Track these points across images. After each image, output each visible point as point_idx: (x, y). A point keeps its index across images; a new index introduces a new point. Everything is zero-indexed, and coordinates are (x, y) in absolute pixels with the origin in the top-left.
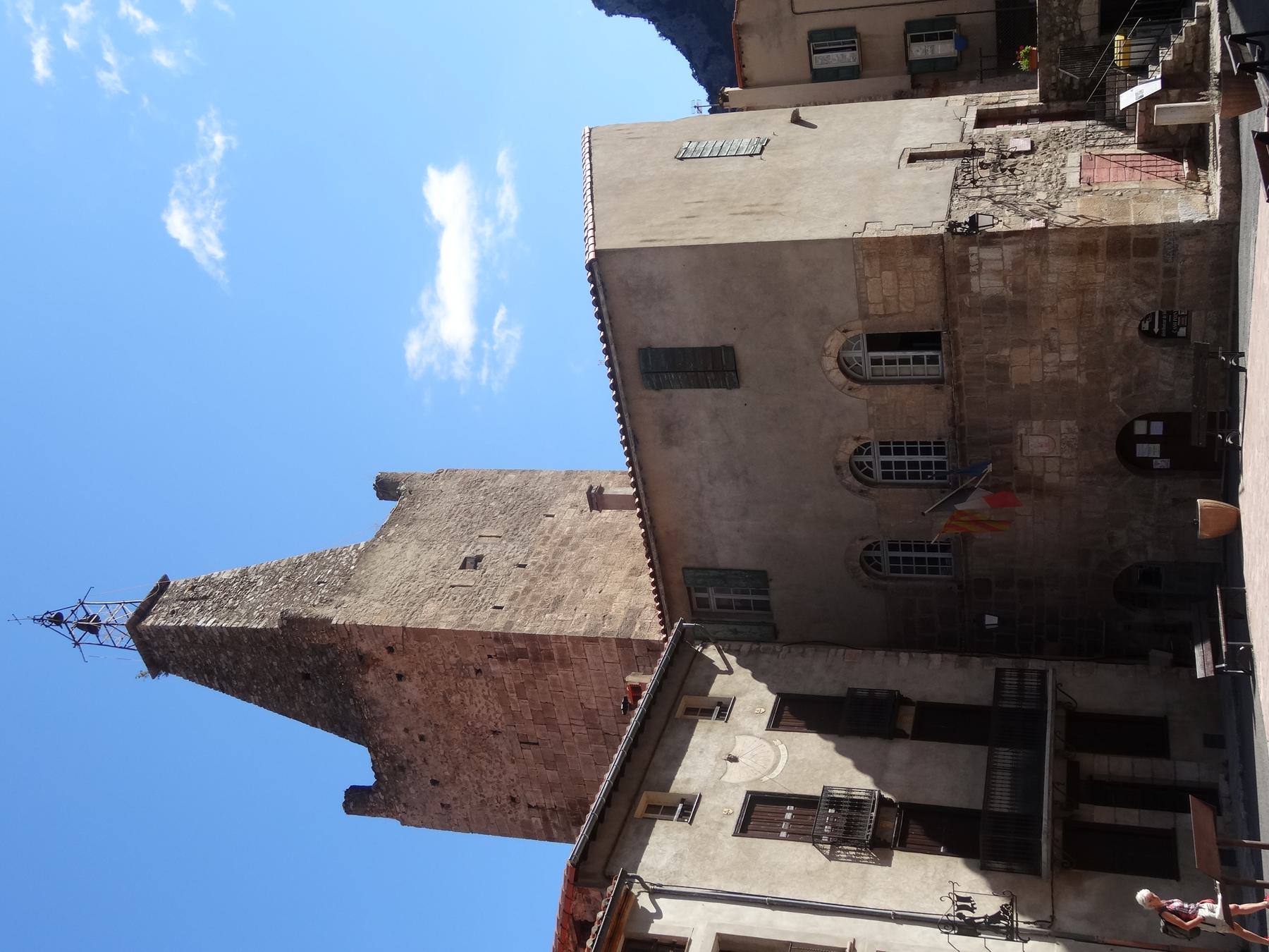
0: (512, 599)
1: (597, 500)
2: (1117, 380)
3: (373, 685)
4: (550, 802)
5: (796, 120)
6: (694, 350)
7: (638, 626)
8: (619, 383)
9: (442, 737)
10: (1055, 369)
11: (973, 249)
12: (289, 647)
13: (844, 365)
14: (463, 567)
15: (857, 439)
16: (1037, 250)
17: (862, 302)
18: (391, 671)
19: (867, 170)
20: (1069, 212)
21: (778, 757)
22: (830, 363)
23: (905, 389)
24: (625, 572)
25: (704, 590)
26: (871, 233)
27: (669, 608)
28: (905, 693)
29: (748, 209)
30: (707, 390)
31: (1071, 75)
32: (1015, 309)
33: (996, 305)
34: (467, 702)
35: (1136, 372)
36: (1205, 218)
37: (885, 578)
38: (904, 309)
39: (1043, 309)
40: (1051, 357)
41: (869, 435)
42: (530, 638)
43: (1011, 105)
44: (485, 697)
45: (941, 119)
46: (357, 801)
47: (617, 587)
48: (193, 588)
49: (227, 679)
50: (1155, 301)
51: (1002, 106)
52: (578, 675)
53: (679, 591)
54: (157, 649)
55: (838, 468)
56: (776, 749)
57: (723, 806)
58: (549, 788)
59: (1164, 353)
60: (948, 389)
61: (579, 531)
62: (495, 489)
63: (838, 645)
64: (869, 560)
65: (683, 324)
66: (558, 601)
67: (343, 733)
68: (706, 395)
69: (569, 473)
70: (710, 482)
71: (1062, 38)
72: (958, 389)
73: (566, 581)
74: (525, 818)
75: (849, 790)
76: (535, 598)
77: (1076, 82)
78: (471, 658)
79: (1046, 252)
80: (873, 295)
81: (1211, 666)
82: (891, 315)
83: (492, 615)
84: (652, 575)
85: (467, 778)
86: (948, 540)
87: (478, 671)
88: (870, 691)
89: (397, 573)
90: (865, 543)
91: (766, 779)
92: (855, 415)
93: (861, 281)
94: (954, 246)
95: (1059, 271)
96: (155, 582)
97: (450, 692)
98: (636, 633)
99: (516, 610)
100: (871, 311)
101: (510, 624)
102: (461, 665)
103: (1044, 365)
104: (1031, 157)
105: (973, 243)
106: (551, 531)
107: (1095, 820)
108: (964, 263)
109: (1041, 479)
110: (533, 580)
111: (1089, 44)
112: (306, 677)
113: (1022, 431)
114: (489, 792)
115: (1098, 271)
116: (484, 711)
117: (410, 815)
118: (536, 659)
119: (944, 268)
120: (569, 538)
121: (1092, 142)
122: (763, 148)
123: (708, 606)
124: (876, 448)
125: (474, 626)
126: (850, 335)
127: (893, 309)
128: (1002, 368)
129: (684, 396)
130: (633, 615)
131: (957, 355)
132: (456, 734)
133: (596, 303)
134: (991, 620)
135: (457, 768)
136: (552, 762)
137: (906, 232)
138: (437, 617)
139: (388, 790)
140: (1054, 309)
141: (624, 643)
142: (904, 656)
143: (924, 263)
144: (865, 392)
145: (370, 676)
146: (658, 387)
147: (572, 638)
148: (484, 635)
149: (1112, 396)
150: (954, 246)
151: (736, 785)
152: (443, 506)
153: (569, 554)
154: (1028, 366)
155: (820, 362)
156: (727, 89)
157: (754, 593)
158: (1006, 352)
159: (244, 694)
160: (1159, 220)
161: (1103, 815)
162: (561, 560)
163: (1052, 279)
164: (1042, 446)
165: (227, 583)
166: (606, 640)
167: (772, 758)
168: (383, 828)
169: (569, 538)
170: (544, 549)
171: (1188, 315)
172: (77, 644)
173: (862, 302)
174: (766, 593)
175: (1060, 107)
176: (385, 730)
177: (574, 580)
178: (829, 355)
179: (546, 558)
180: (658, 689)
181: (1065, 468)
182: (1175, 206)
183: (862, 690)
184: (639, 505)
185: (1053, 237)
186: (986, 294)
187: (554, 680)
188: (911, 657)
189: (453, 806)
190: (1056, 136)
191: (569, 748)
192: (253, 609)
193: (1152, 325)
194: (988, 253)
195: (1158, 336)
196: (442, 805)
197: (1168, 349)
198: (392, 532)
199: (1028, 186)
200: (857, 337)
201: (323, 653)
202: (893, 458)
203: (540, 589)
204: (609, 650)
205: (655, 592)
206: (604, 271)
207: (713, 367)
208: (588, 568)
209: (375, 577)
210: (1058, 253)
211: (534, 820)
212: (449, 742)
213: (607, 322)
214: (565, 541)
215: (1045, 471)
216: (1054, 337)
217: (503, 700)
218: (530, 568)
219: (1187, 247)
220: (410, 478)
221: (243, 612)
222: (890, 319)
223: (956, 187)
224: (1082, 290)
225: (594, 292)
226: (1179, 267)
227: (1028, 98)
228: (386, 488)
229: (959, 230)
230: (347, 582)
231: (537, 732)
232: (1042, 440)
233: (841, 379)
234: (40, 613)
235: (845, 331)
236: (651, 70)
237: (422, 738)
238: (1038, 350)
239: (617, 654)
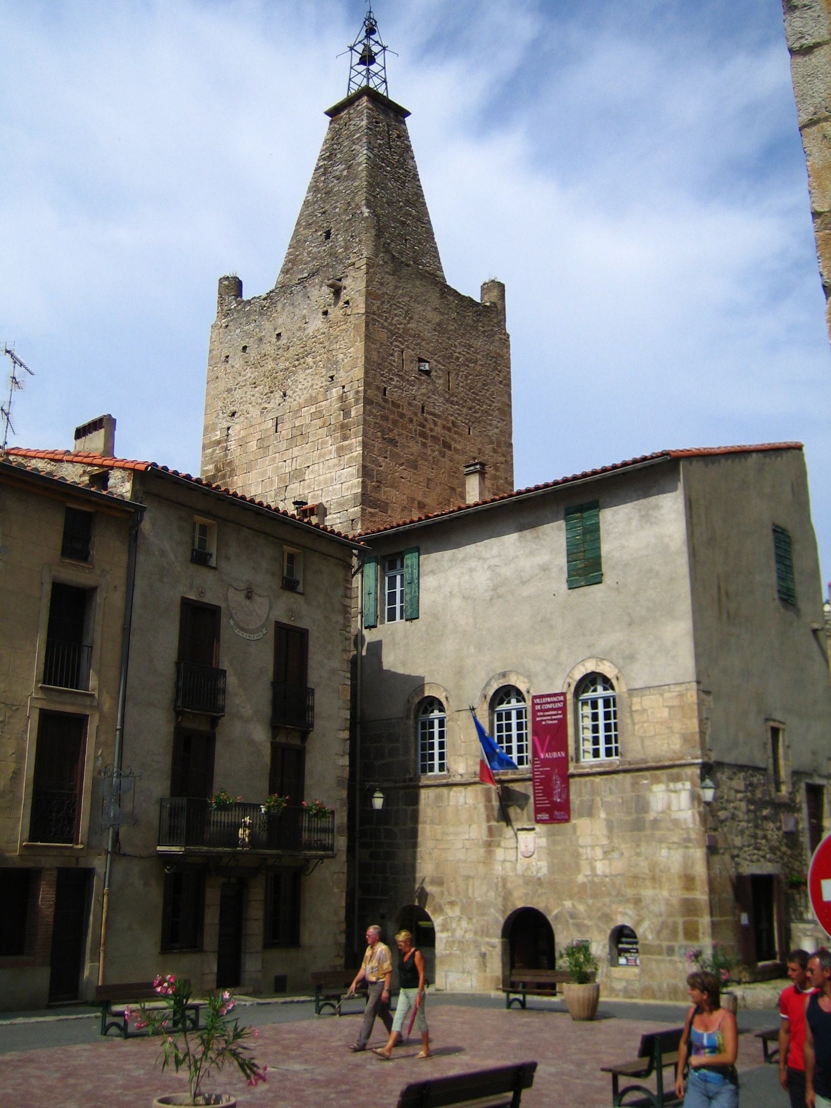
2: (581, 908)
4: (232, 445)
6: (599, 548)
7: (372, 510)
10: (590, 856)
11: (688, 785)
16: (688, 840)
28: (312, 735)
29: (723, 591)
30: (565, 560)
33: (642, 806)
34: (308, 371)
35: (587, 922)
37: (416, 718)
38: (637, 727)
39: (638, 846)
40: (599, 852)
41: (620, 688)
50: (646, 938)
54: (349, 113)
55: (504, 675)
57: (208, 588)
63: (353, 678)
66: (393, 442)
68: (562, 560)
70: (489, 567)
76: (395, 422)
79: (687, 847)
80: (649, 701)
82: (632, 716)
83: (378, 388)
85: (249, 375)
87: (332, 377)
88: (312, 708)
100: (635, 700)
103: (593, 847)
105: (693, 784)
106: (456, 433)
109: (499, 846)
110: (411, 420)
112: (328, 235)
116: (300, 386)
118: (343, 427)
120: (450, 448)
126: (614, 682)
127: (637, 718)
134: (378, 802)
139: (238, 311)
140: (638, 854)
142: (346, 734)
149: (568, 904)
151: (226, 599)
157: (402, 607)
158: (603, 815)
161: (213, 897)
162: (429, 442)
163: (664, 852)
169: (450, 448)
170: (438, 430)
172: (352, 48)
174: (402, 618)
178: (597, 665)
187: (326, 443)
188: (345, 740)
189: (228, 366)
191: (274, 459)
196: (227, 357)
202: (514, 721)
203: (404, 427)
210: (686, 858)
216: (616, 855)
217: (312, 401)
222: (628, 715)
231: (285, 430)
234: (375, 15)
235: (617, 679)
237: (279, 335)
238: (605, 842)
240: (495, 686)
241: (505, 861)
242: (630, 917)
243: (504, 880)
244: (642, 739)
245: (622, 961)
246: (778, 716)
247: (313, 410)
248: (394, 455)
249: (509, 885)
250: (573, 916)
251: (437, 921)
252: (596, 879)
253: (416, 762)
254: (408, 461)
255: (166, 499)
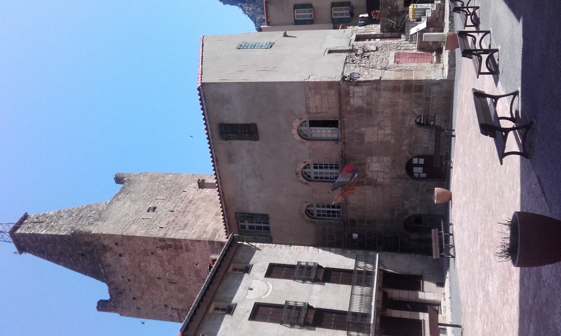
0: (167, 224)
1: (202, 185)
2: (406, 141)
3: (109, 258)
5: (285, 35)
6: (240, 124)
8: (210, 137)
9: (137, 280)
11: (351, 87)
12: (76, 242)
13: (300, 133)
14: (148, 211)
15: (305, 162)
16: (376, 89)
17: (308, 107)
18: (117, 253)
19: (312, 56)
20: (389, 76)
21: (269, 289)
22: (294, 132)
23: (324, 143)
24: (213, 215)
25: (244, 222)
26: (312, 79)
27: (229, 228)
29: (264, 69)
31: (392, 22)
32: (367, 112)
33: (360, 110)
34: (148, 266)
36: (442, 78)
37: (315, 218)
40: (381, 132)
41: (309, 161)
42: (174, 240)
43: (369, 33)
44: (155, 264)
45: (343, 37)
46: (103, 306)
47: (210, 220)
48: (37, 218)
49: (50, 255)
51: (366, 33)
52: (193, 255)
53: (233, 221)
55: (297, 174)
56: (268, 285)
58: (181, 301)
59: (425, 131)
60: (341, 143)
61: (196, 197)
62: (163, 181)
64: (309, 211)
65: (237, 115)
66: (186, 225)
67: (97, 278)
68: (245, 143)
69: (193, 175)
70: (246, 178)
71: (389, 7)
72: (344, 143)
73: (190, 217)
74: (171, 313)
75: (296, 302)
76: (177, 224)
77: (395, 25)
78: (149, 248)
79: (380, 89)
80: (312, 105)
81: (438, 254)
83: (159, 231)
84: (223, 215)
86: (339, 204)
87: (152, 253)
89: (121, 213)
90: (307, 204)
91: (263, 297)
92: (305, 154)
93: (307, 99)
94: (344, 86)
95: (385, 97)
96: (21, 215)
97: (141, 262)
98: (217, 239)
99: (169, 229)
100: (311, 111)
101: (166, 234)
102: (145, 250)
103: (378, 134)
104: (376, 52)
105: (351, 85)
106: (185, 197)
107: (393, 316)
108: (348, 93)
109: (376, 180)
110: (176, 217)
111: (400, 10)
112: (83, 255)
113: (369, 161)
114: (156, 303)
115: (400, 98)
116: (155, 270)
117: (124, 311)
118: (176, 248)
119: (340, 95)
120: (191, 201)
121: (399, 48)
122: (271, 46)
123: (245, 228)
124: (312, 166)
125: (151, 235)
126: (303, 120)
127: (319, 111)
128: (362, 135)
129: (236, 144)
130: (216, 231)
131: (344, 129)
132: (143, 278)
133: (201, 104)
135: (143, 293)
136: (182, 290)
137: (325, 79)
138: (136, 231)
140: (383, 112)
141: (211, 243)
143: (332, 92)
144: (308, 143)
145: (108, 255)
146: (226, 139)
147: (190, 240)
148: (155, 238)
149: (404, 148)
150: (344, 86)
152: (143, 186)
153: (191, 206)
154: (372, 135)
155: (290, 131)
156: (262, 26)
157: (263, 223)
158: (363, 129)
159: (57, 262)
160: (424, 78)
161: (396, 313)
163: (382, 100)
164: (377, 167)
165: (52, 217)
166: (204, 241)
167: (266, 288)
168: (113, 317)
170: (182, 205)
171: (435, 116)
173: (308, 107)
174: (268, 223)
175: (389, 34)
176: (114, 277)
177: (193, 217)
179: (182, 208)
180: (222, 260)
181: (385, 176)
182: (430, 73)
183: (303, 262)
184: (218, 187)
185: (383, 84)
186: (356, 106)
190: (386, 45)
191: (189, 285)
192: (62, 227)
193: (420, 120)
194: (357, 89)
195: (423, 124)
196: (137, 308)
197: (426, 130)
198: (120, 196)
199: (374, 64)
200: (305, 122)
201: (89, 245)
203: (179, 220)
204: (205, 245)
205: (224, 222)
206: (205, 91)
207: (248, 132)
208: (199, 212)
209: (111, 214)
210: (385, 90)
211: (174, 314)
212: (140, 282)
213: (206, 112)
214: (190, 202)
215: (378, 177)
216: (382, 124)
217: (162, 264)
218: (175, 212)
219: (435, 89)
220: (129, 175)
221: (57, 228)
223: (346, 63)
224: (394, 105)
225: (201, 99)
226: (431, 97)
227: (375, 29)
228: (119, 180)
229: (346, 79)
230: (100, 217)
231: (176, 278)
232: (377, 165)
233: (298, 138)
236: (239, 21)
237: (129, 280)
238: (376, 128)
239: (208, 247)
240: (302, 178)
241: (384, 178)
242: (411, 118)
243: (393, 178)
244: (329, 108)
245: (432, 123)
246: (323, 51)
247: (167, 263)
248: (192, 226)
249: (395, 176)
250: (410, 146)
251: (411, 212)
252: (393, 134)
253: (336, 220)
254: (195, 219)
255: (199, 325)
